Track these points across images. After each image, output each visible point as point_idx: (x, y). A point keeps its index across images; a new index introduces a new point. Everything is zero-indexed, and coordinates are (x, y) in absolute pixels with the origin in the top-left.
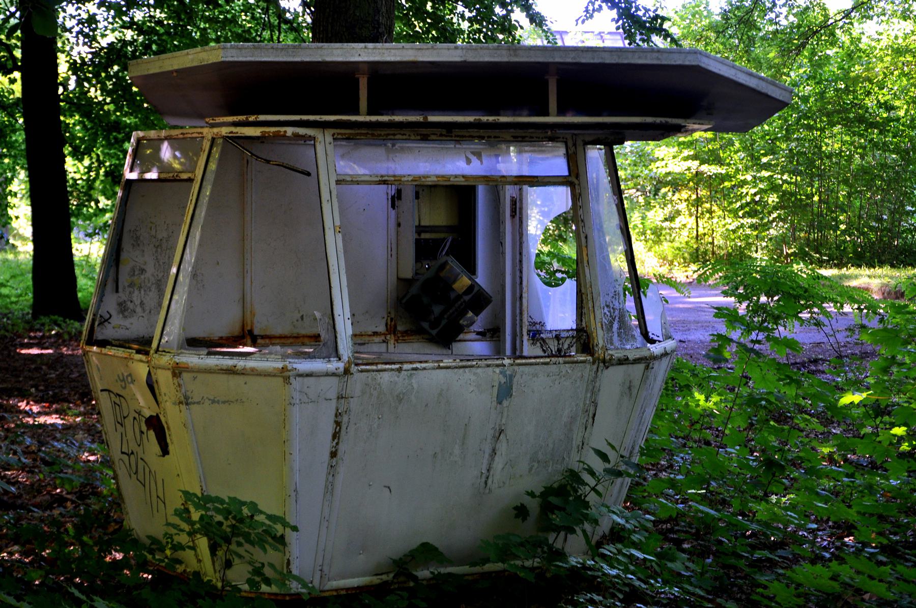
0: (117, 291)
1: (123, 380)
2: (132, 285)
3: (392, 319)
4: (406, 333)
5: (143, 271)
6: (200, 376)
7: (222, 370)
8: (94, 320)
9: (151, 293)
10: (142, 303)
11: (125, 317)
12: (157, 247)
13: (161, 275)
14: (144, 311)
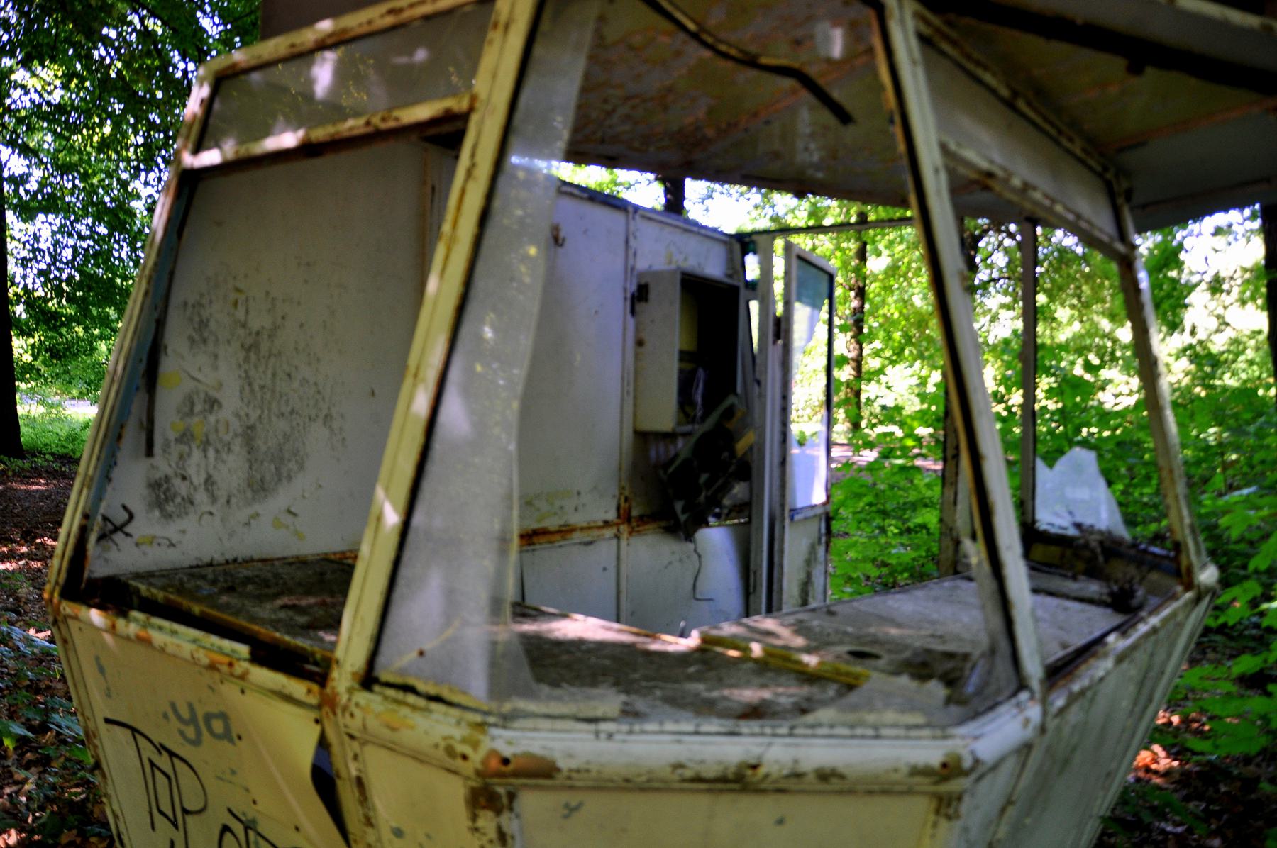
0: (149, 452)
1: (193, 720)
2: (185, 437)
3: (626, 499)
4: (642, 519)
5: (213, 403)
6: (594, 804)
7: (698, 779)
8: (84, 531)
9: (231, 459)
10: (209, 482)
11: (168, 516)
12: (248, 350)
13: (254, 415)
14: (214, 499)
